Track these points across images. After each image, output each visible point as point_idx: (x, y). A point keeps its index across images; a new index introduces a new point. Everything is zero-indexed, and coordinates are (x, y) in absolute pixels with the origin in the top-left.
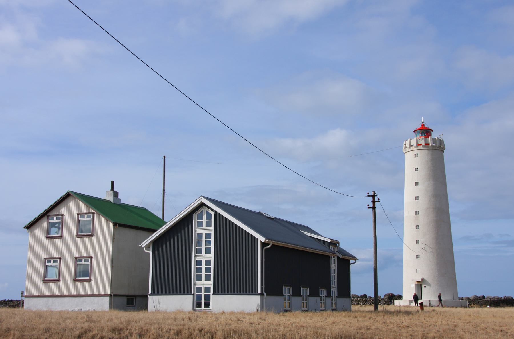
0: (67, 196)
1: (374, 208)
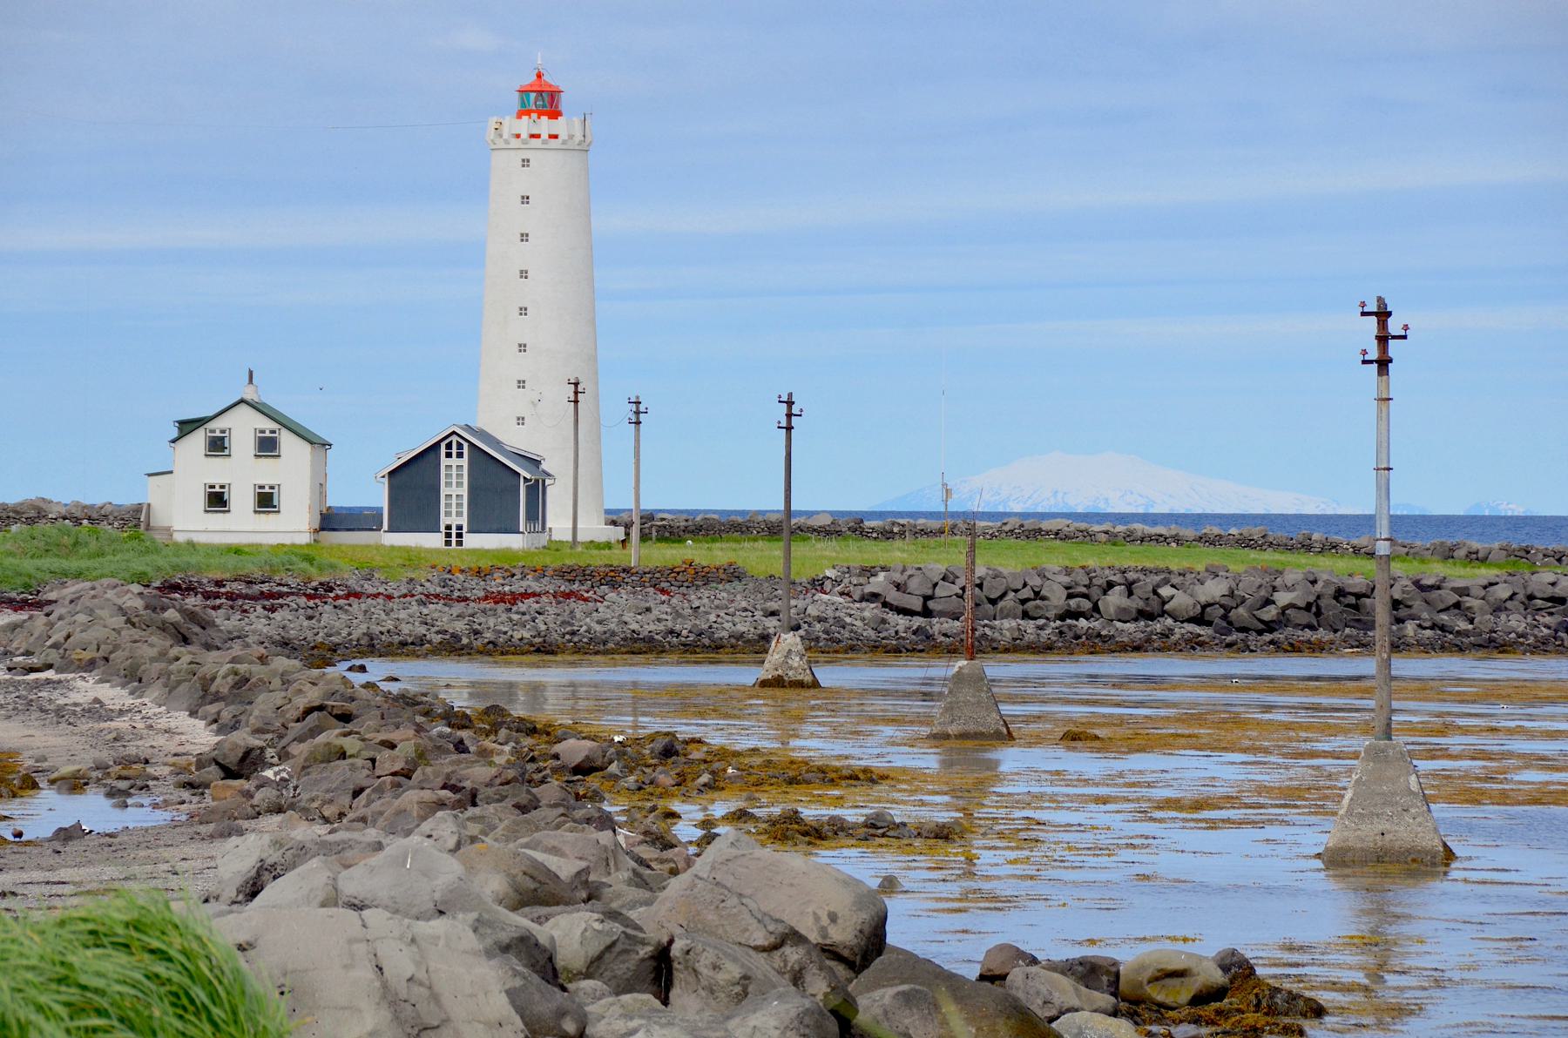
0: (242, 401)
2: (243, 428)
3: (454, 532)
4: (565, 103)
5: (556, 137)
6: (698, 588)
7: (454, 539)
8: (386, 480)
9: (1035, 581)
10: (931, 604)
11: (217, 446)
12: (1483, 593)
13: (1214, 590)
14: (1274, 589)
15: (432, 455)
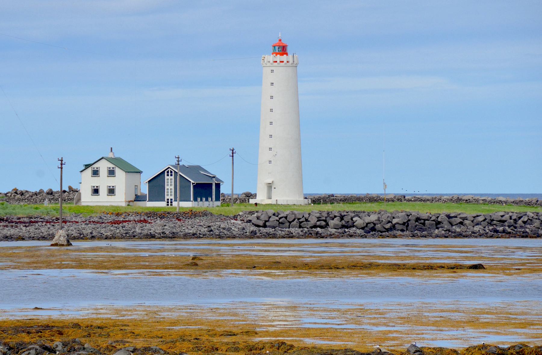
0: (103, 158)
1: (233, 156)
2: (104, 167)
3: (170, 201)
4: (289, 50)
5: (283, 62)
7: (170, 203)
8: (147, 184)
9: (306, 216)
10: (267, 224)
11: (96, 173)
12: (473, 219)
13: (373, 218)
14: (394, 218)
15: (162, 175)
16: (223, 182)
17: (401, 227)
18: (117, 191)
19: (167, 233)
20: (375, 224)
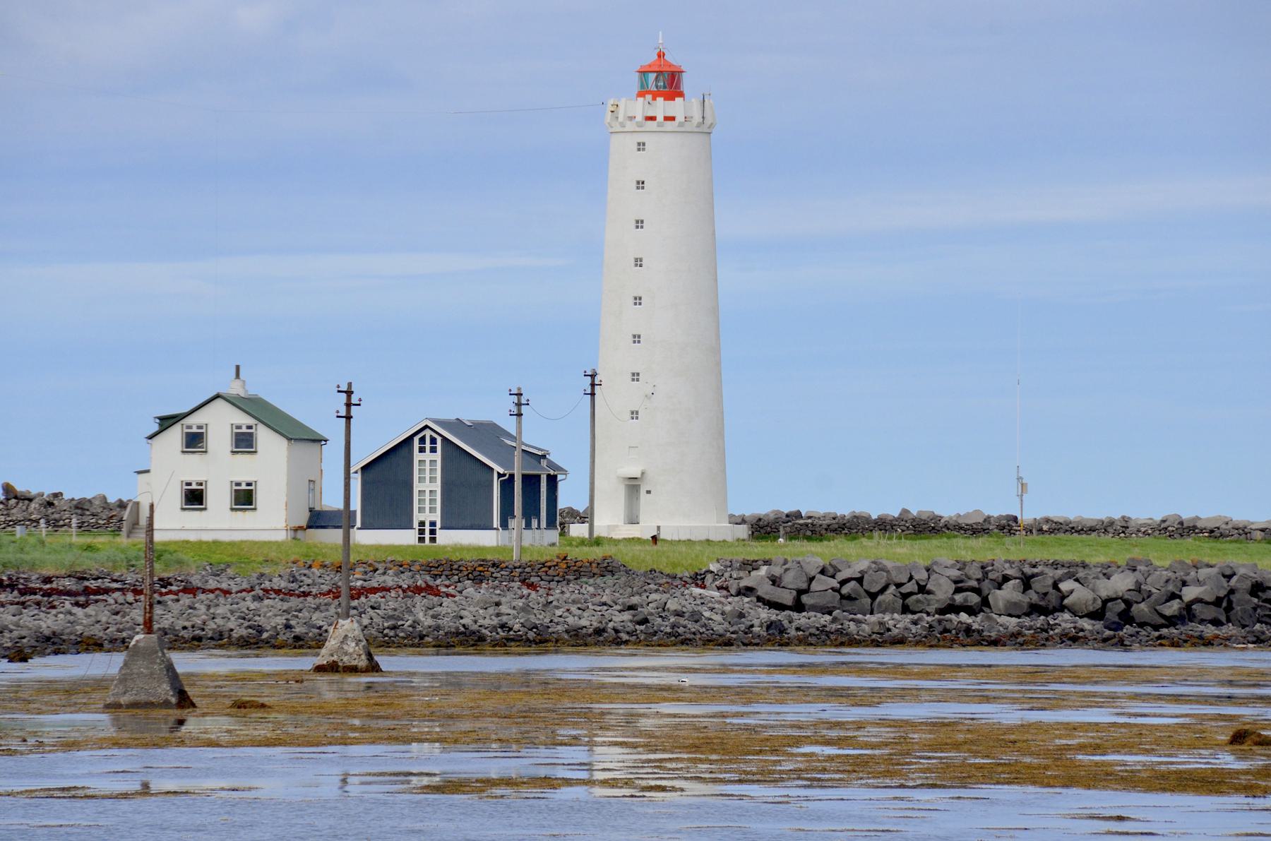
0: (217, 396)
1: (593, 394)
2: (220, 423)
3: (427, 528)
4: (687, 84)
5: (673, 119)
6: (569, 582)
7: (427, 536)
9: (921, 575)
10: (805, 599)
11: (194, 441)
13: (1121, 583)
14: (1184, 584)
15: (404, 451)
16: (564, 472)
17: (1211, 612)
18: (260, 498)
19: (517, 627)
20: (1128, 603)
